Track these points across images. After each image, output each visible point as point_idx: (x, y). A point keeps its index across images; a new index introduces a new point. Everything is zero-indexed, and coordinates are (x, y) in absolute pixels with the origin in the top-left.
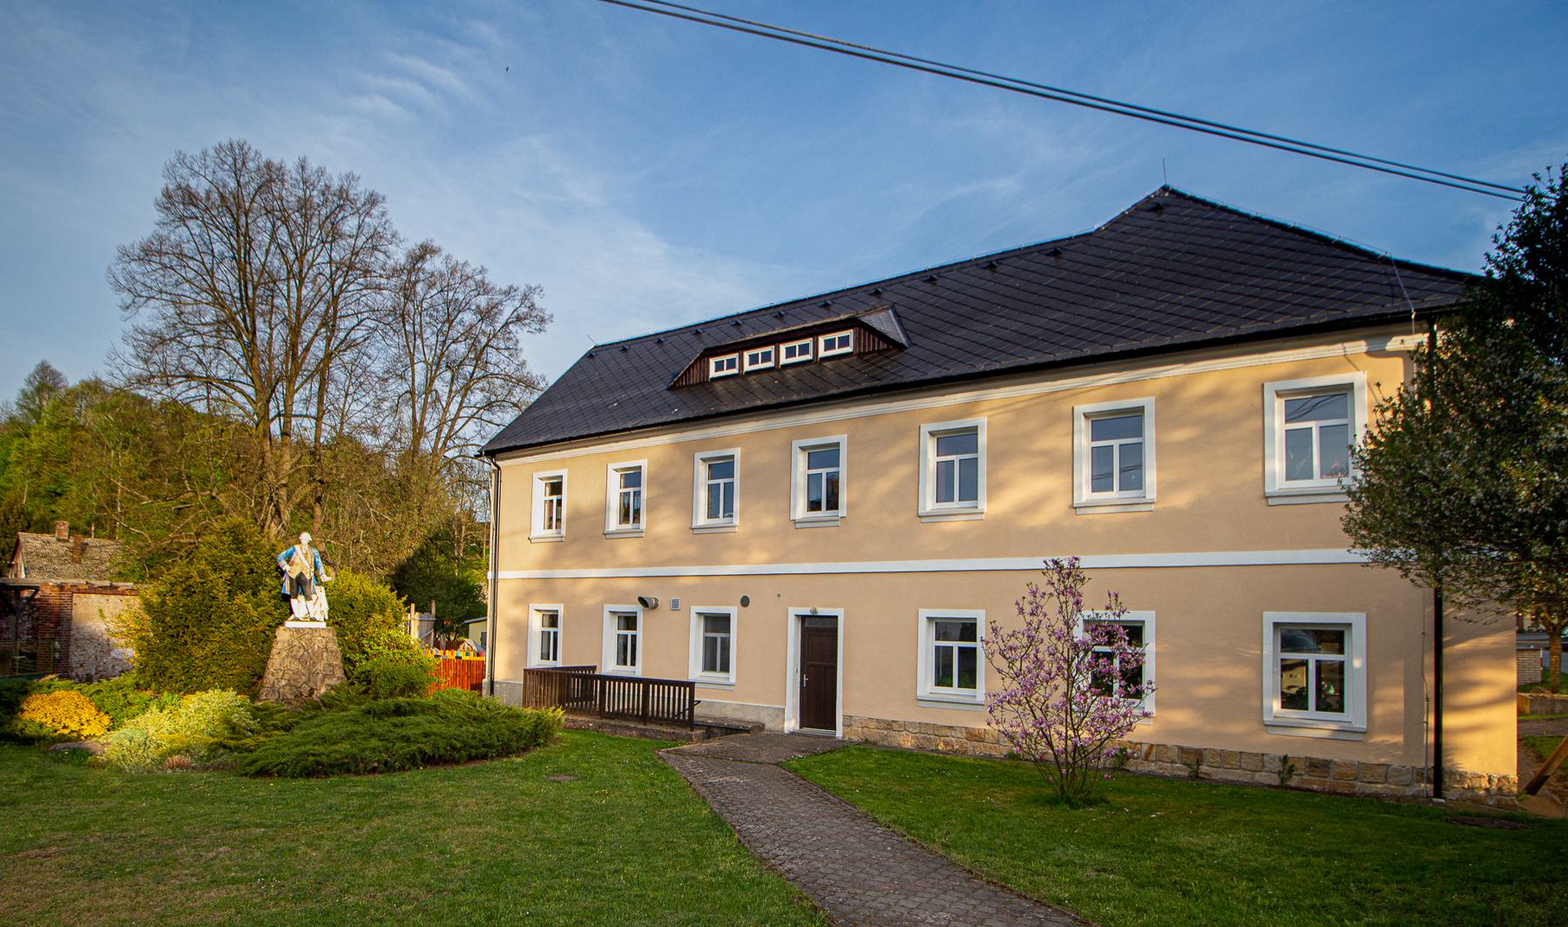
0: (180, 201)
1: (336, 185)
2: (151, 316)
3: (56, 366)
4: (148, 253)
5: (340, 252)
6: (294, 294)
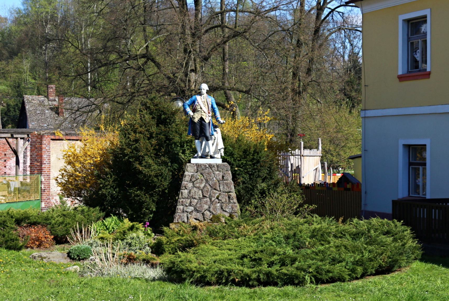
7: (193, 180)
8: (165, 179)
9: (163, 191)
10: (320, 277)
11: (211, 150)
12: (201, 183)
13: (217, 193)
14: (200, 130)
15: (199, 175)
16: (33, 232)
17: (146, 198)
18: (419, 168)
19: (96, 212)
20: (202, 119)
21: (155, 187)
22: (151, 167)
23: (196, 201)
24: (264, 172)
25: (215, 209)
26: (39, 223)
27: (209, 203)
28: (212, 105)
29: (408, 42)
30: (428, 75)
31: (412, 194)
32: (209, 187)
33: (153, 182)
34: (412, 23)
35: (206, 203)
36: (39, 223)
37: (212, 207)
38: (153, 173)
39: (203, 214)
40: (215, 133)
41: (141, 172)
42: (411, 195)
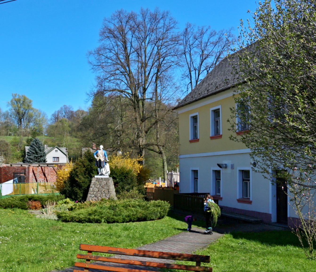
7: (95, 184)
8: (86, 184)
9: (85, 188)
10: (108, 220)
11: (104, 173)
12: (98, 185)
13: (104, 190)
14: (100, 164)
15: (97, 183)
16: (34, 203)
17: (79, 191)
18: (247, 182)
19: (63, 196)
20: (100, 160)
21: (82, 187)
22: (81, 179)
23: (95, 193)
24: (129, 181)
25: (102, 196)
26: (38, 200)
27: (100, 193)
28: (105, 154)
29: (214, 121)
30: (221, 136)
31: (245, 196)
32: (101, 187)
33: (81, 185)
34: (216, 112)
35: (99, 193)
36: (38, 200)
37: (101, 195)
38: (81, 181)
39: (98, 198)
40: (106, 165)
41: (77, 181)
42: (244, 197)
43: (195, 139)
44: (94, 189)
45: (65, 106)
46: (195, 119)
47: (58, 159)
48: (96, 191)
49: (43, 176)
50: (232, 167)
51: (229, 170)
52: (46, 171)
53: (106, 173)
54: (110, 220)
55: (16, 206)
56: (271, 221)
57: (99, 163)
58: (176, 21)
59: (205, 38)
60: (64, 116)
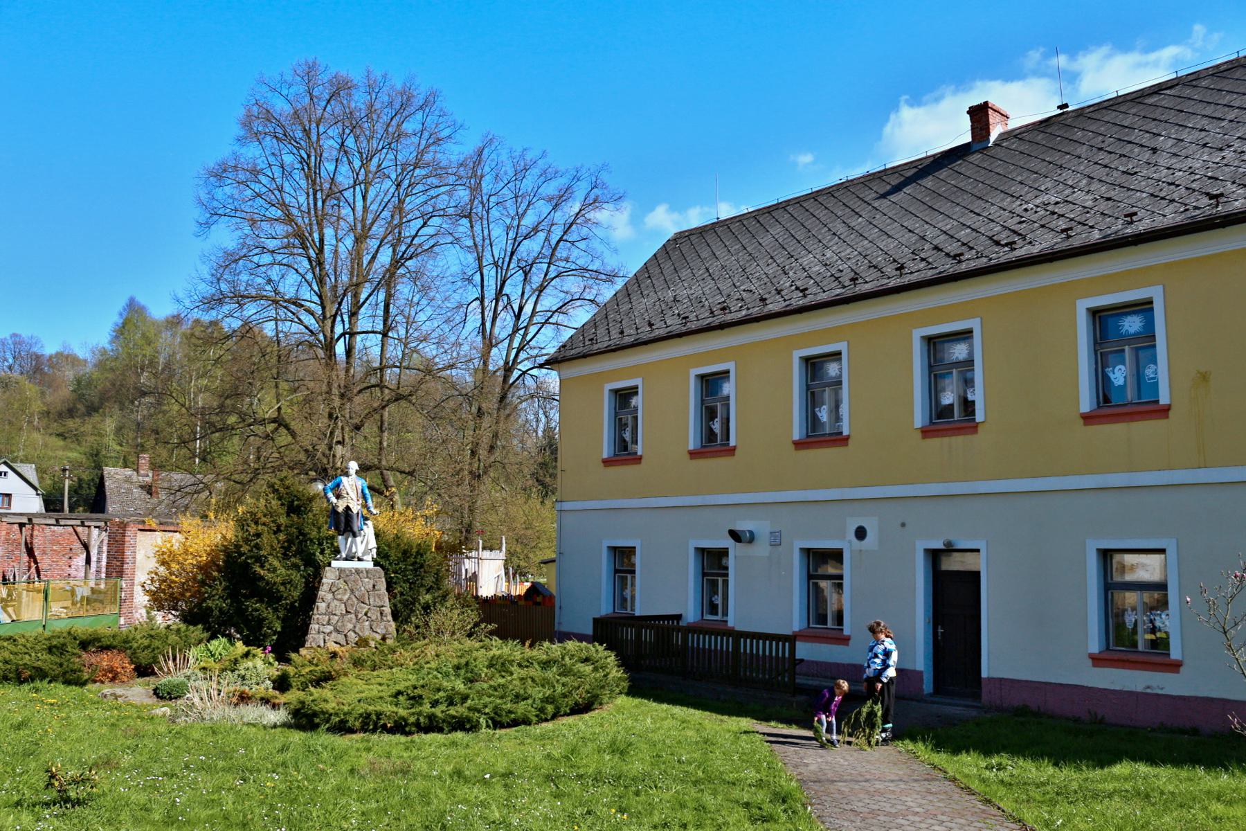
0: (259, 122)
1: (399, 87)
2: (226, 236)
3: (142, 299)
4: (220, 173)
5: (407, 152)
6: (359, 204)
9: (292, 604)
14: (345, 523)
15: (341, 584)
16: (104, 660)
19: (197, 631)
20: (348, 508)
22: (276, 571)
25: (362, 629)
26: (114, 647)
33: (279, 591)
35: (350, 621)
36: (114, 647)
37: (358, 626)
38: (279, 580)
41: (262, 578)
43: (624, 453)
44: (333, 605)
45: (15, 335)
46: (623, 397)
47: (6, 499)
48: (338, 612)
49: (25, 558)
50: (776, 540)
51: (761, 549)
52: (35, 541)
53: (364, 554)
54: (505, 720)
55: (40, 674)
56: (922, 690)
57: (343, 518)
58: (460, 122)
59: (528, 184)
60: (10, 368)
